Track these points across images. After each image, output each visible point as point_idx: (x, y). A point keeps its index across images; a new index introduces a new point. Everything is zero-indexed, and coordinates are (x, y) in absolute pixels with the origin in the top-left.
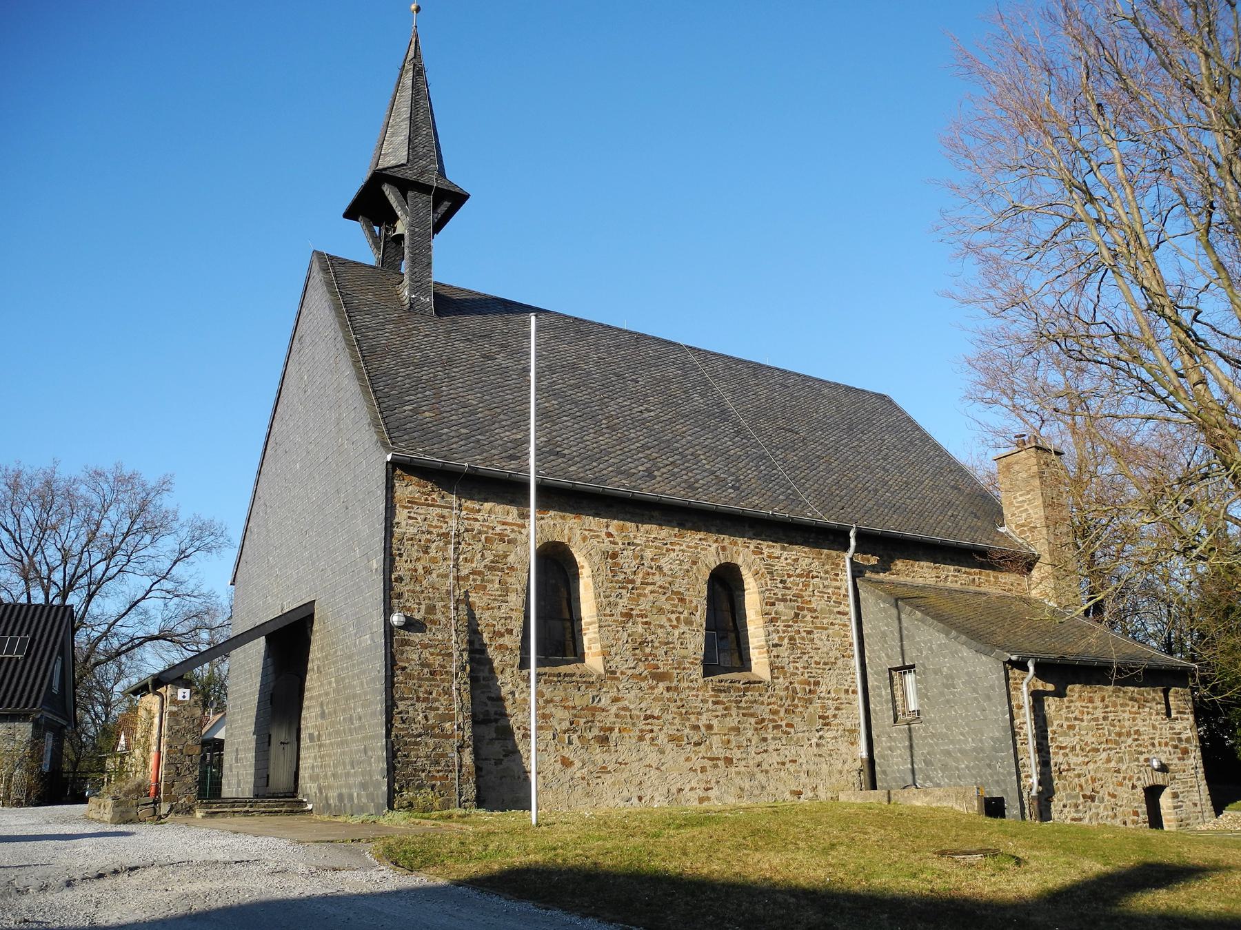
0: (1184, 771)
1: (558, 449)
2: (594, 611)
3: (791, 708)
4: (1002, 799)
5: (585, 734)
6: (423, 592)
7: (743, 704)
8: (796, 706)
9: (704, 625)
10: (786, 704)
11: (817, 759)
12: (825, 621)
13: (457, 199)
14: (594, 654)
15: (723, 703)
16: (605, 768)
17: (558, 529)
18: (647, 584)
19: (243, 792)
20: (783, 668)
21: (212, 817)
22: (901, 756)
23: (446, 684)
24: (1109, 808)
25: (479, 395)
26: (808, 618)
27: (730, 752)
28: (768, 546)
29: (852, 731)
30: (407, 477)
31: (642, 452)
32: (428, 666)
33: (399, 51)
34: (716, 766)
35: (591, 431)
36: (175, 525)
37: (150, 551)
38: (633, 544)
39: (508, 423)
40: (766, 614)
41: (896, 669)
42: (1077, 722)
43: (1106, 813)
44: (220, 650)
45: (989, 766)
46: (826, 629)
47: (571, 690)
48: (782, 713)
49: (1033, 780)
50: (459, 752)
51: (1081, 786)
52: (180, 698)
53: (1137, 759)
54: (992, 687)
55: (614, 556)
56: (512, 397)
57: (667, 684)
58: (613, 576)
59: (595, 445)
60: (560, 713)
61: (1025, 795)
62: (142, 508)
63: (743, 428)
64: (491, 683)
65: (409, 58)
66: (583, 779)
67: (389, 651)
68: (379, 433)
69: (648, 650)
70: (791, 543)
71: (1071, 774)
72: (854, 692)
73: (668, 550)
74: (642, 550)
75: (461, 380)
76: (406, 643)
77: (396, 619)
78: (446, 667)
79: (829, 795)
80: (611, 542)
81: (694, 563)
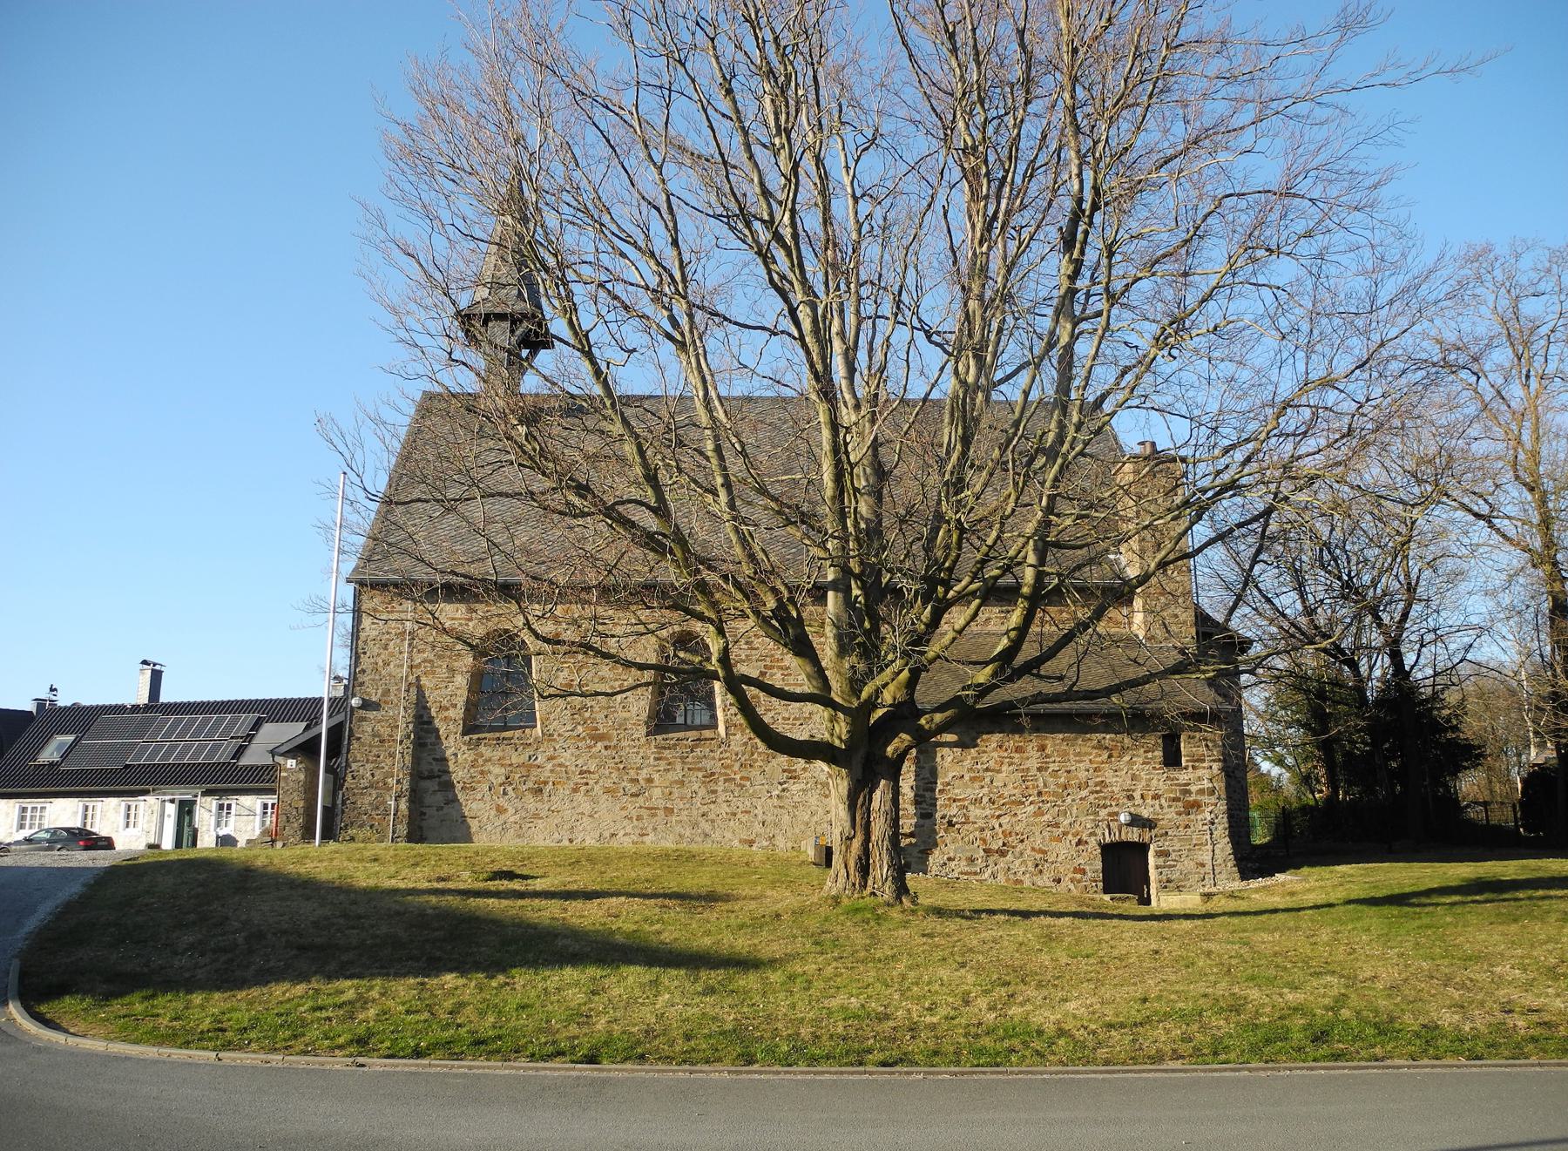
7: (689, 760)
24: (1030, 864)
32: (379, 736)
34: (654, 815)
51: (984, 841)
60: (497, 770)
69: (587, 715)
76: (363, 719)
79: (790, 845)
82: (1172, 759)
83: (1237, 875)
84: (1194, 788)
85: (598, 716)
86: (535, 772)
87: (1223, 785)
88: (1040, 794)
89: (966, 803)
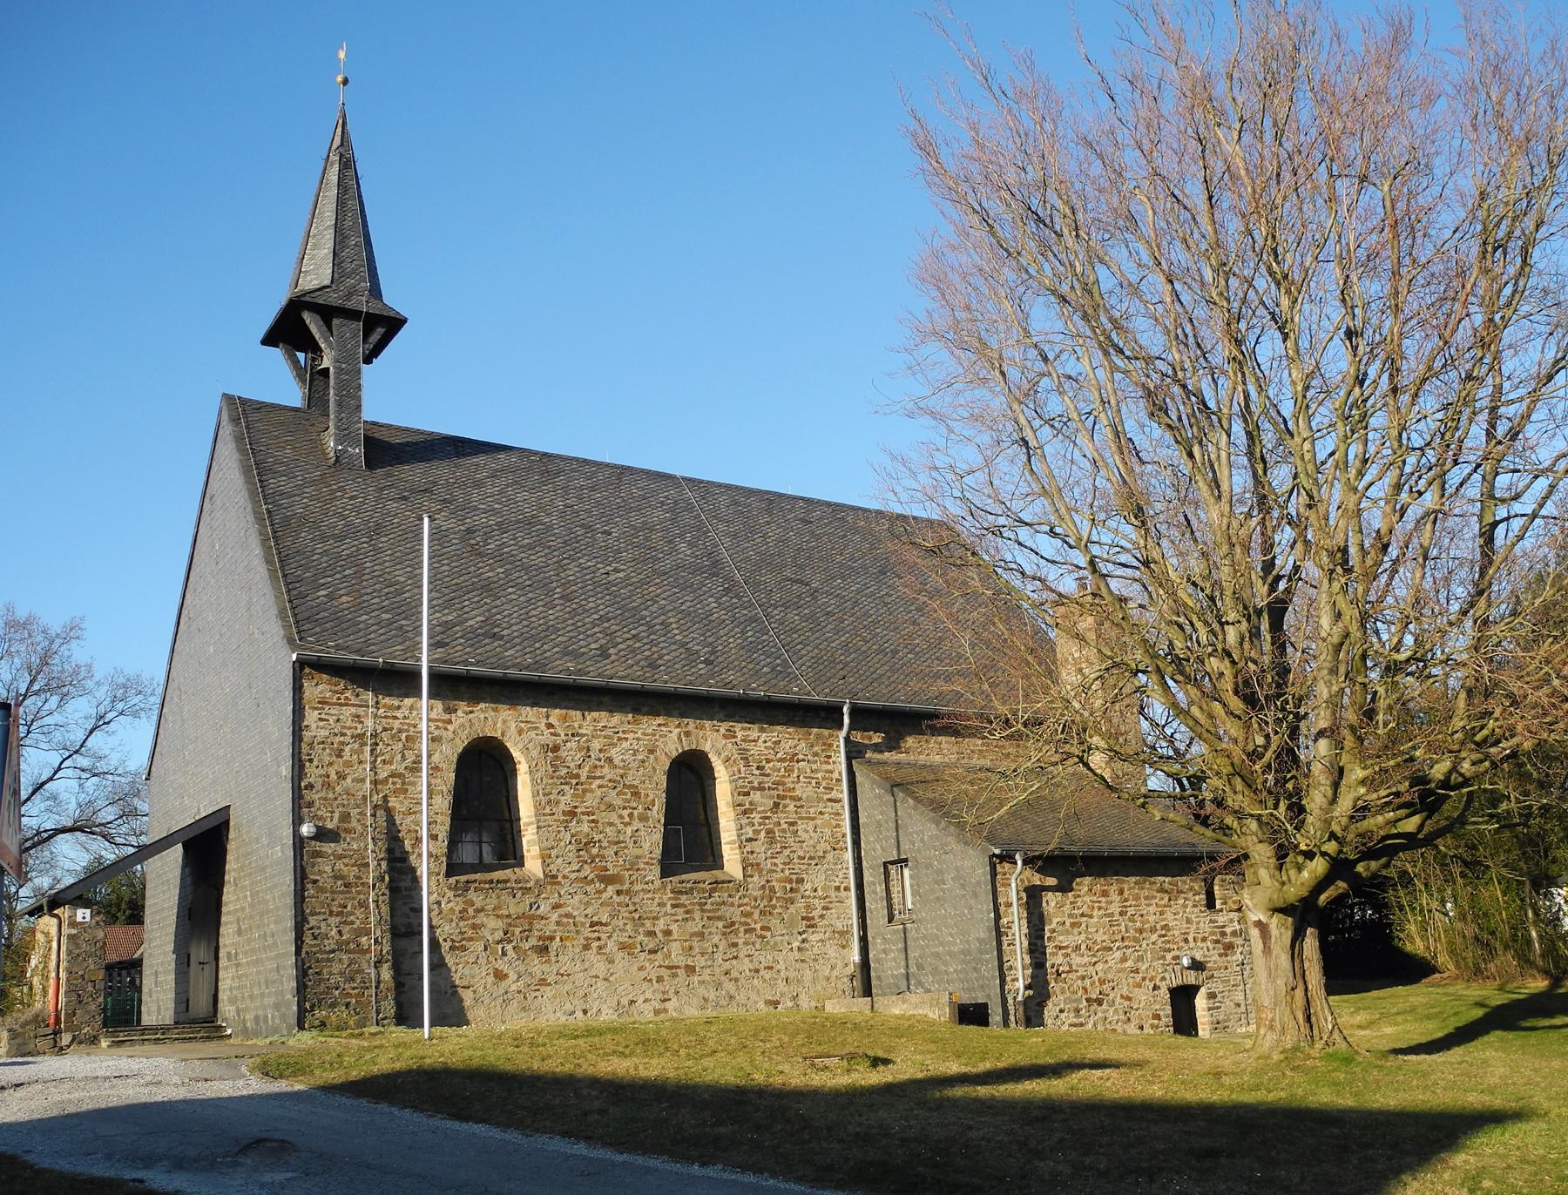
0: (1226, 968)
1: (496, 630)
2: (532, 811)
3: (768, 909)
4: (986, 1005)
5: (521, 945)
6: (336, 799)
7: (708, 907)
8: (774, 907)
9: (663, 821)
10: (762, 905)
11: (799, 965)
12: (812, 810)
13: (394, 324)
14: (533, 858)
15: (684, 906)
16: (544, 980)
17: (490, 722)
18: (594, 778)
19: (163, 1020)
20: (758, 864)
21: (118, 1046)
22: (894, 959)
23: (362, 896)
24: (1121, 1012)
25: (409, 569)
26: (791, 808)
27: (692, 959)
28: (743, 729)
29: (844, 933)
30: (317, 676)
31: (598, 625)
32: (342, 877)
33: (322, 139)
34: (675, 976)
35: (540, 603)
36: (89, 684)
37: (56, 718)
38: (578, 735)
39: (440, 601)
40: (738, 805)
41: (892, 863)
42: (1085, 919)
43: (1116, 1017)
44: (146, 852)
45: (975, 969)
46: (813, 819)
47: (505, 896)
48: (756, 916)
49: (1019, 984)
50: (376, 967)
51: (1085, 989)
52: (79, 919)
53: (1164, 957)
54: (978, 883)
55: (556, 749)
56: (448, 568)
57: (618, 887)
58: (554, 772)
59: (542, 621)
60: (492, 923)
61: (1010, 1001)
62: (44, 662)
63: (735, 584)
64: (413, 893)
65: (335, 146)
66: (519, 992)
67: (298, 864)
68: (286, 627)
69: (595, 851)
70: (772, 724)
71: (1073, 976)
72: (847, 889)
73: (620, 739)
74: (588, 741)
75: (389, 552)
76: (318, 854)
77: (306, 830)
78: (362, 879)
79: (813, 1004)
80: (552, 734)
81: (652, 752)
84: (1228, 930)
85: (606, 852)
86: (537, 925)
89: (1069, 950)
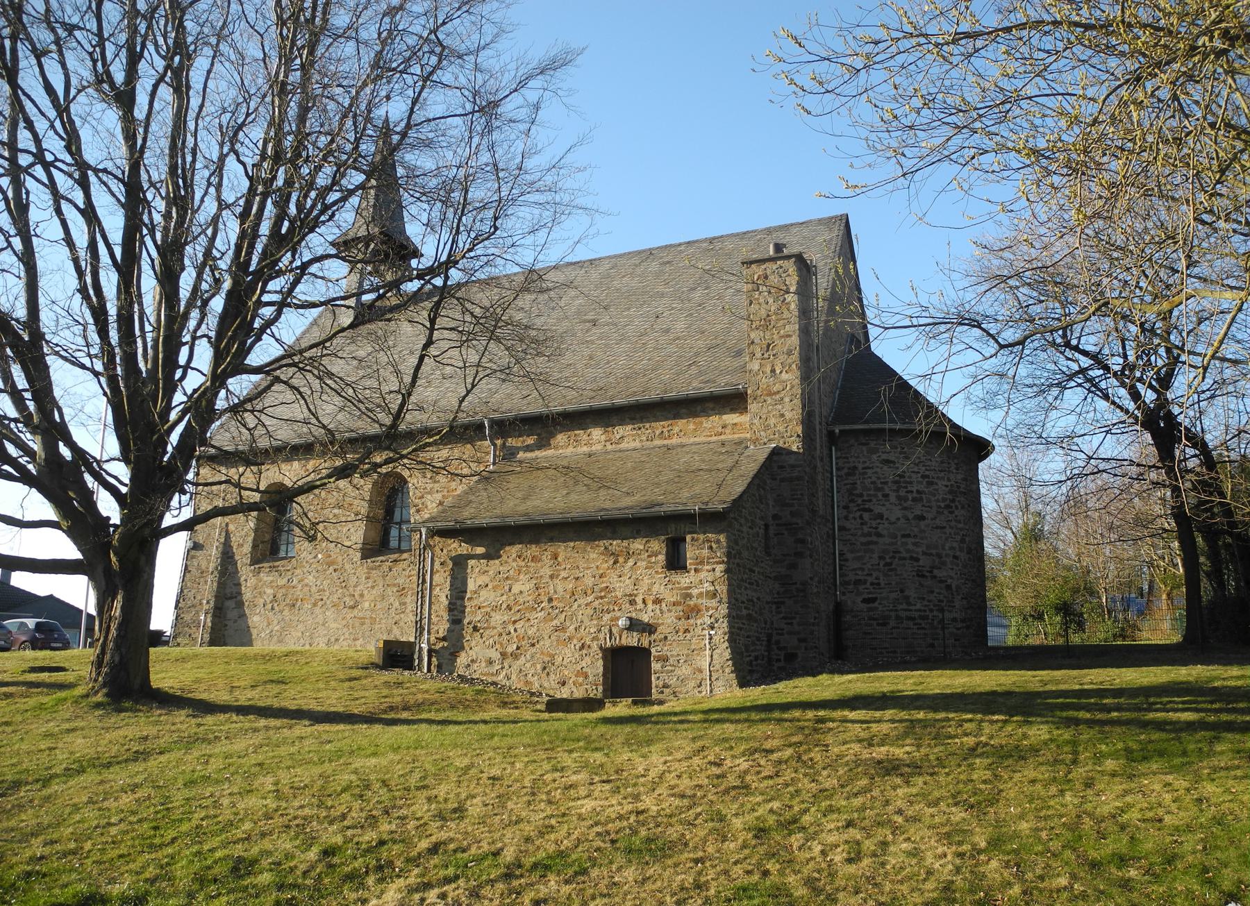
24: (539, 666)
34: (363, 624)
82: (675, 563)
83: (735, 682)
84: (695, 592)
87: (725, 588)
88: (550, 600)
